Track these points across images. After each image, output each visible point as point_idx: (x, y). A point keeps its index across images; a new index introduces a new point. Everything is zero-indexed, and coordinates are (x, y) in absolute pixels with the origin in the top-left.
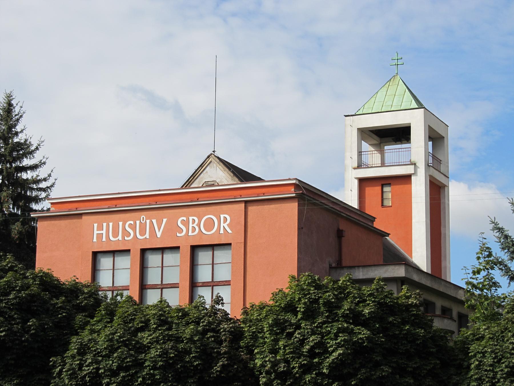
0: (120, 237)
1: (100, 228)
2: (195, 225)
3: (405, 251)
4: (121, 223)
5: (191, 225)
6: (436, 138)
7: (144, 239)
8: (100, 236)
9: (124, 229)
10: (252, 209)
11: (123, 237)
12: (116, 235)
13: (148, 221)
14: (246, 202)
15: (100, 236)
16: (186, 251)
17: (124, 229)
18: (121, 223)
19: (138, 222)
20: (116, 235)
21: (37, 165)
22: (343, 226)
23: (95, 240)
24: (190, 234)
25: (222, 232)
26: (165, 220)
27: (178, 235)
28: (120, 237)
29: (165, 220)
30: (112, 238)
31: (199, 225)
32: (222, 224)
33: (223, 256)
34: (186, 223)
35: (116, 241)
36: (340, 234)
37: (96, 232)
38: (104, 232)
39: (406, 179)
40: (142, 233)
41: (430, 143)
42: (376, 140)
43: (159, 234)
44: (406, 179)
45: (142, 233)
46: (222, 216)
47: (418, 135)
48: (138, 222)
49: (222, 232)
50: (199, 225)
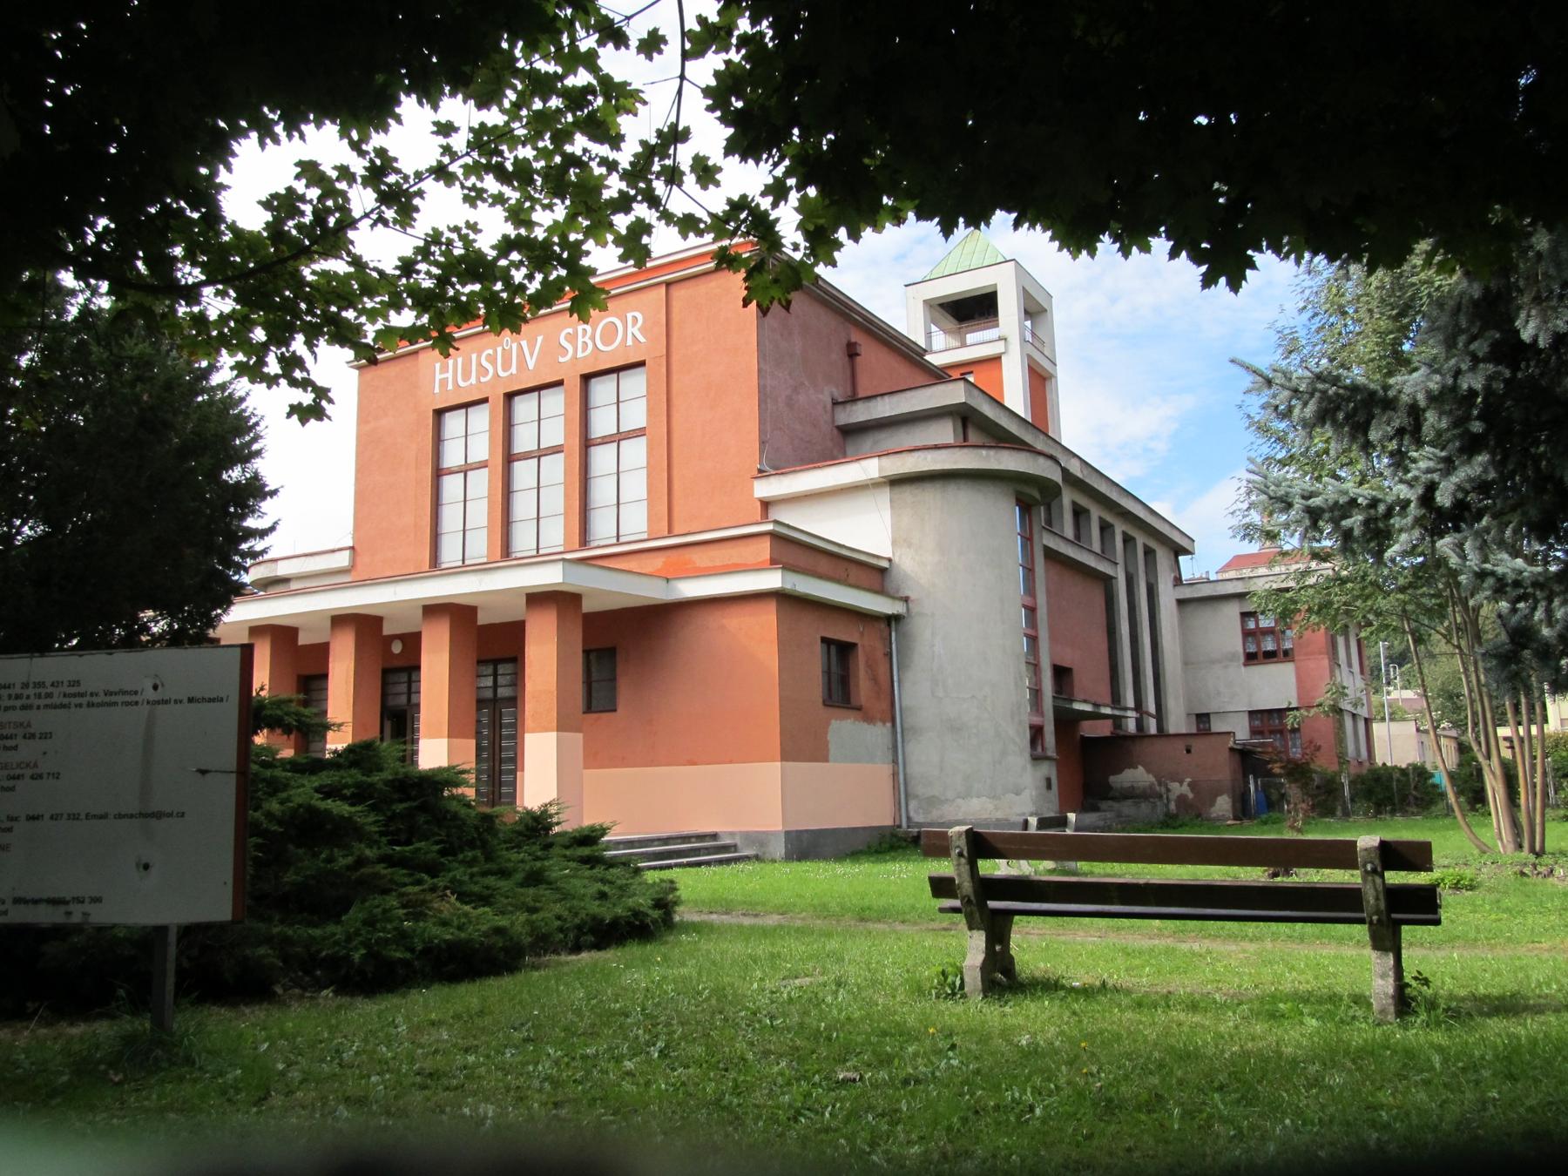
0: (473, 380)
1: (444, 369)
2: (587, 339)
3: (1123, 830)
4: (474, 357)
5: (580, 340)
6: (1034, 310)
7: (511, 376)
8: (444, 382)
9: (480, 364)
10: (679, 293)
11: (478, 379)
12: (466, 376)
13: (515, 346)
14: (668, 284)
15: (444, 382)
16: (574, 384)
17: (480, 364)
18: (474, 357)
19: (499, 350)
20: (466, 376)
21: (1091, 987)
22: (856, 336)
23: (437, 390)
24: (580, 355)
25: (630, 343)
26: (540, 339)
27: (561, 360)
28: (473, 380)
29: (540, 339)
30: (462, 384)
31: (593, 338)
32: (630, 330)
33: (635, 384)
34: (572, 338)
35: (469, 386)
36: (852, 352)
37: (438, 377)
38: (450, 375)
39: (996, 359)
40: (506, 366)
41: (1028, 323)
42: (951, 323)
43: (531, 364)
44: (996, 359)
45: (506, 366)
46: (629, 316)
47: (1009, 306)
48: (499, 350)
49: (630, 343)
50: (593, 338)
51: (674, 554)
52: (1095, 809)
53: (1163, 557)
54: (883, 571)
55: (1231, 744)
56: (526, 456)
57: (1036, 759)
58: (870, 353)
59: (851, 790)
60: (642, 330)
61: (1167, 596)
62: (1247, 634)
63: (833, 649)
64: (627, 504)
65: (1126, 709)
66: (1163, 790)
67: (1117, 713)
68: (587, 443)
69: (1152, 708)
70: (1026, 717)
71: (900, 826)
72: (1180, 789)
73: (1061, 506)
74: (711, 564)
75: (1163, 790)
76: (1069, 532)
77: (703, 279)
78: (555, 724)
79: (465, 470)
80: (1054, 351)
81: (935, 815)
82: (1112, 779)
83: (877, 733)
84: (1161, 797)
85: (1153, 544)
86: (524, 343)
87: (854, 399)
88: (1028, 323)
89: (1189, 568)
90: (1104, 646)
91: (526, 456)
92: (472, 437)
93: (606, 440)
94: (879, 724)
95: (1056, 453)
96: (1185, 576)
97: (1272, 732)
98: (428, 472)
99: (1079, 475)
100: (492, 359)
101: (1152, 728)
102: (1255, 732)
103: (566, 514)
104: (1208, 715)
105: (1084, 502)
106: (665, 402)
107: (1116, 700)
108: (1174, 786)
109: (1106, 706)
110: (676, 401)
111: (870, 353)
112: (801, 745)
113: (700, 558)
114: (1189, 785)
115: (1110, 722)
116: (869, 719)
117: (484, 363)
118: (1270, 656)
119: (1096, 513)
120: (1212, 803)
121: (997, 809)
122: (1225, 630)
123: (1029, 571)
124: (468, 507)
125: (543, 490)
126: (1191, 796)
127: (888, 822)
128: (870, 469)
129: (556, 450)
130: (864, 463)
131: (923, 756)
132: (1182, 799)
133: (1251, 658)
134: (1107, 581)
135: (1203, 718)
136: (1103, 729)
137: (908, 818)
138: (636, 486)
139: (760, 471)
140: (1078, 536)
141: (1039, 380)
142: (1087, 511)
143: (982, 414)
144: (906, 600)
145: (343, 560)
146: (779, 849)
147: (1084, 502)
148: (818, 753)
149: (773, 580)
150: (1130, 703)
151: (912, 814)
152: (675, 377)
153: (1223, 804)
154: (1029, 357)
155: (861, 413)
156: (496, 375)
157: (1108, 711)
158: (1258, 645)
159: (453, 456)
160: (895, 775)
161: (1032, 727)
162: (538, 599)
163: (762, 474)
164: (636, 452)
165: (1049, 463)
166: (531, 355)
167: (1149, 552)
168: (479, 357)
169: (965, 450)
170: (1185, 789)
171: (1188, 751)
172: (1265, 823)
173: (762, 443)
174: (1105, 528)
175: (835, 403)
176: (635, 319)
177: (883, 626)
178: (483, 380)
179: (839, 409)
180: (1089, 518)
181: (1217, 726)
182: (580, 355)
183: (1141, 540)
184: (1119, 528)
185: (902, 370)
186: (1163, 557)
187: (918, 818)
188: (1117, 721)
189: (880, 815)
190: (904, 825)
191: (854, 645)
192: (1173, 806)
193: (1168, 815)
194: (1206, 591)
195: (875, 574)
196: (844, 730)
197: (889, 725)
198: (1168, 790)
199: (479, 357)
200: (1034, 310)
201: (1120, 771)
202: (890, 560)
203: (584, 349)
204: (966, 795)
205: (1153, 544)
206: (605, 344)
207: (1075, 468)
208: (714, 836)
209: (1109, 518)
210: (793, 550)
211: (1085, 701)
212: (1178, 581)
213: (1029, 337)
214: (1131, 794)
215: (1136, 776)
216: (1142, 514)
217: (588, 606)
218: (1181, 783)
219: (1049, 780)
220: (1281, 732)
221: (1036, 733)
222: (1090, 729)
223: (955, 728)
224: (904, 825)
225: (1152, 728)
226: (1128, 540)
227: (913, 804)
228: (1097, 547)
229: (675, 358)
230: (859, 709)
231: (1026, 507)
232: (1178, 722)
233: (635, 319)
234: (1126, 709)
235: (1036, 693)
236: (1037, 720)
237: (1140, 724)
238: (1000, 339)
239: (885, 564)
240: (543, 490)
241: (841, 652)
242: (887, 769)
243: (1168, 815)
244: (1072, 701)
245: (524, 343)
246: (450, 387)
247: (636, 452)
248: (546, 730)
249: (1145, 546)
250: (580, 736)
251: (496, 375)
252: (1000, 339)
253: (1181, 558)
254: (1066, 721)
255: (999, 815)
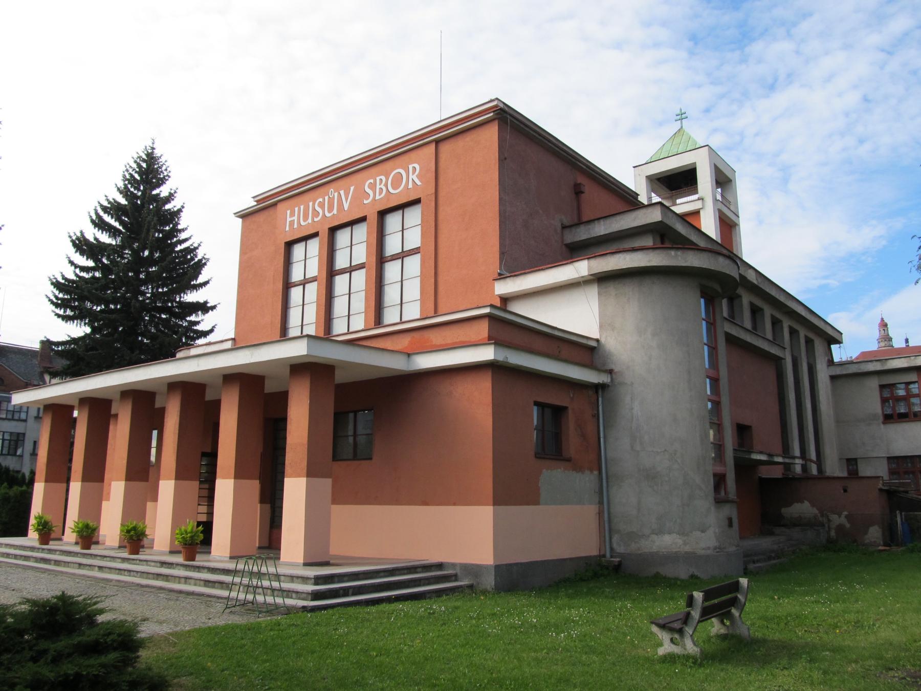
0: (310, 221)
2: (382, 186)
4: (311, 204)
5: (378, 187)
9: (314, 209)
10: (445, 148)
11: (313, 219)
13: (336, 194)
15: (292, 223)
16: (373, 218)
17: (314, 209)
18: (311, 204)
19: (327, 198)
22: (581, 179)
23: (287, 229)
24: (378, 197)
25: (410, 186)
26: (352, 188)
27: (365, 202)
28: (310, 221)
29: (352, 188)
30: (303, 223)
33: (414, 216)
34: (373, 186)
36: (578, 191)
37: (289, 219)
38: (295, 218)
39: (696, 213)
40: (331, 209)
41: (719, 190)
43: (346, 206)
45: (331, 209)
46: (411, 167)
47: (705, 179)
48: (327, 198)
49: (410, 186)
51: (416, 335)
52: (772, 534)
53: (819, 346)
54: (592, 349)
55: (880, 486)
56: (342, 272)
57: (719, 502)
58: (591, 191)
59: (562, 528)
60: (419, 177)
61: (823, 374)
62: (884, 401)
63: (548, 412)
64: (406, 300)
65: (794, 458)
66: (825, 520)
67: (787, 461)
68: (381, 260)
69: (813, 456)
70: (711, 468)
71: (604, 556)
72: (838, 520)
73: (741, 306)
74: (443, 343)
75: (825, 520)
76: (748, 324)
77: (460, 137)
78: (305, 471)
79: (304, 283)
80: (737, 208)
81: (633, 547)
82: (784, 510)
83: (585, 481)
84: (823, 525)
85: (811, 335)
86: (342, 192)
87: (580, 223)
88: (719, 190)
89: (839, 353)
90: (776, 409)
91: (342, 272)
92: (307, 261)
93: (394, 258)
94: (587, 472)
95: (735, 259)
96: (836, 359)
97: (906, 473)
98: (280, 286)
99: (755, 282)
100: (322, 205)
101: (814, 470)
102: (892, 472)
103: (366, 312)
104: (856, 460)
105: (759, 303)
106: (434, 229)
107: (786, 450)
108: (834, 517)
109: (777, 455)
110: (441, 226)
111: (591, 191)
112: (511, 490)
113: (436, 337)
114: (846, 517)
115: (781, 467)
116: (578, 468)
117: (317, 208)
118: (903, 417)
119: (768, 311)
120: (866, 533)
121: (685, 544)
122: (869, 399)
123: (713, 349)
124: (304, 311)
125: (352, 294)
126: (848, 525)
127: (595, 553)
128: (581, 268)
129: (361, 266)
130: (577, 264)
131: (626, 498)
132: (840, 528)
133: (888, 418)
134: (777, 361)
135: (852, 463)
136: (776, 473)
137: (612, 549)
138: (413, 290)
139: (500, 274)
140: (755, 327)
141: (728, 225)
142: (761, 310)
143: (675, 231)
144: (611, 372)
145: (228, 345)
146: (489, 581)
147: (759, 303)
148: (530, 497)
149: (487, 354)
150: (797, 453)
151: (615, 546)
152: (441, 209)
153: (875, 533)
154: (720, 211)
155: (582, 234)
156: (324, 215)
157: (780, 460)
158: (894, 408)
159: (297, 274)
160: (600, 513)
161: (715, 475)
162: (298, 368)
163: (501, 277)
164: (414, 264)
165: (727, 262)
166: (346, 200)
167: (809, 342)
168: (314, 204)
169: (658, 251)
170: (843, 520)
171: (845, 491)
172: (912, 551)
173: (502, 253)
174: (776, 323)
175: (564, 227)
176: (414, 168)
177: (591, 393)
178: (316, 220)
179: (567, 231)
180: (763, 315)
181: (866, 470)
182: (378, 197)
183: (803, 332)
184: (786, 323)
185: (616, 204)
186: (819, 346)
187: (620, 549)
188: (787, 467)
189: (589, 547)
190: (608, 555)
191: (566, 408)
192: (833, 533)
193: (830, 541)
194: (853, 369)
195: (584, 351)
196: (553, 476)
197: (596, 473)
198: (829, 521)
199: (314, 204)
200: (723, 180)
201: (789, 505)
202: (597, 341)
203: (381, 193)
204: (660, 532)
205: (811, 335)
206: (394, 188)
207: (751, 277)
208: (440, 566)
209: (778, 315)
210: (504, 326)
211: (761, 453)
212: (831, 362)
213: (719, 197)
214: (799, 523)
215: (803, 509)
216: (803, 313)
217: (340, 377)
218: (840, 516)
219: (730, 521)
220: (913, 473)
221: (719, 480)
222: (766, 472)
223: (650, 476)
224: (608, 555)
225: (814, 470)
226: (793, 332)
227: (616, 538)
228: (769, 335)
229: (442, 194)
230: (569, 460)
231: (710, 299)
232: (834, 467)
233: (414, 168)
234: (794, 458)
235: (719, 447)
236: (719, 469)
237: (805, 468)
238: (699, 199)
239: (594, 344)
240: (352, 294)
241: (554, 415)
242: (591, 510)
243: (830, 541)
244: (750, 452)
245: (342, 192)
246: (296, 226)
247: (414, 264)
248: (299, 476)
249: (806, 337)
250: (328, 482)
251: (324, 215)
252: (699, 199)
253: (832, 346)
254: (745, 468)
255: (687, 549)
